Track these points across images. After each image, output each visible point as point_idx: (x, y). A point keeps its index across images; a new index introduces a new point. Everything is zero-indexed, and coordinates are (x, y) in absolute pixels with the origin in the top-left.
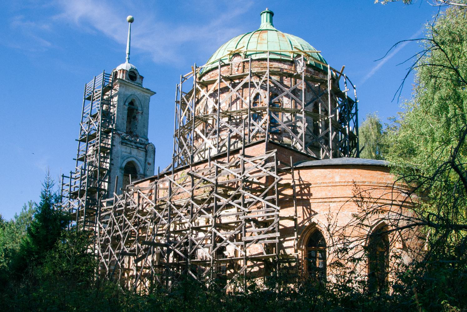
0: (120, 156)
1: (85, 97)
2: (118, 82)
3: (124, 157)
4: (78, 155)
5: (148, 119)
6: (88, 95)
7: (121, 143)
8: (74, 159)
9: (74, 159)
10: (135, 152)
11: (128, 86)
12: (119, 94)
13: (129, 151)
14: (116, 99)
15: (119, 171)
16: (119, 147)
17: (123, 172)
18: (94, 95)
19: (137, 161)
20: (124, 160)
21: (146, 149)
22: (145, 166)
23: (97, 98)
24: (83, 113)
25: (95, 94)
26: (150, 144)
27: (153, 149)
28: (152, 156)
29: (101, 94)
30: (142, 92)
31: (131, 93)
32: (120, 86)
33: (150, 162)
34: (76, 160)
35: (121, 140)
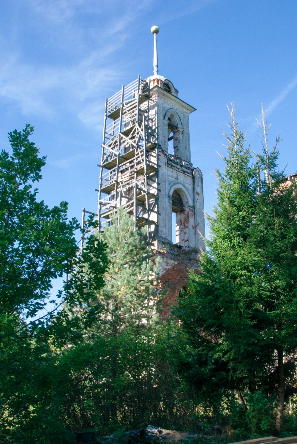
0: (167, 181)
1: (106, 114)
2: (156, 91)
3: (171, 182)
4: (101, 185)
5: (189, 139)
6: (109, 112)
7: (166, 163)
8: (96, 190)
9: (96, 190)
10: (182, 177)
11: (166, 98)
12: (157, 105)
13: (175, 176)
14: (152, 112)
15: (167, 199)
16: (165, 170)
17: (171, 202)
18: (124, 108)
19: (184, 190)
20: (171, 187)
21: (192, 175)
22: (194, 197)
23: (128, 111)
24: (105, 133)
25: (126, 106)
26: (197, 169)
27: (200, 176)
28: (200, 185)
29: (137, 104)
30: (181, 107)
31: (169, 107)
32: (158, 96)
33: (198, 192)
34: (98, 191)
35: (166, 160)
